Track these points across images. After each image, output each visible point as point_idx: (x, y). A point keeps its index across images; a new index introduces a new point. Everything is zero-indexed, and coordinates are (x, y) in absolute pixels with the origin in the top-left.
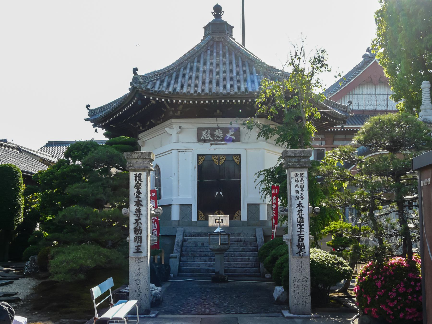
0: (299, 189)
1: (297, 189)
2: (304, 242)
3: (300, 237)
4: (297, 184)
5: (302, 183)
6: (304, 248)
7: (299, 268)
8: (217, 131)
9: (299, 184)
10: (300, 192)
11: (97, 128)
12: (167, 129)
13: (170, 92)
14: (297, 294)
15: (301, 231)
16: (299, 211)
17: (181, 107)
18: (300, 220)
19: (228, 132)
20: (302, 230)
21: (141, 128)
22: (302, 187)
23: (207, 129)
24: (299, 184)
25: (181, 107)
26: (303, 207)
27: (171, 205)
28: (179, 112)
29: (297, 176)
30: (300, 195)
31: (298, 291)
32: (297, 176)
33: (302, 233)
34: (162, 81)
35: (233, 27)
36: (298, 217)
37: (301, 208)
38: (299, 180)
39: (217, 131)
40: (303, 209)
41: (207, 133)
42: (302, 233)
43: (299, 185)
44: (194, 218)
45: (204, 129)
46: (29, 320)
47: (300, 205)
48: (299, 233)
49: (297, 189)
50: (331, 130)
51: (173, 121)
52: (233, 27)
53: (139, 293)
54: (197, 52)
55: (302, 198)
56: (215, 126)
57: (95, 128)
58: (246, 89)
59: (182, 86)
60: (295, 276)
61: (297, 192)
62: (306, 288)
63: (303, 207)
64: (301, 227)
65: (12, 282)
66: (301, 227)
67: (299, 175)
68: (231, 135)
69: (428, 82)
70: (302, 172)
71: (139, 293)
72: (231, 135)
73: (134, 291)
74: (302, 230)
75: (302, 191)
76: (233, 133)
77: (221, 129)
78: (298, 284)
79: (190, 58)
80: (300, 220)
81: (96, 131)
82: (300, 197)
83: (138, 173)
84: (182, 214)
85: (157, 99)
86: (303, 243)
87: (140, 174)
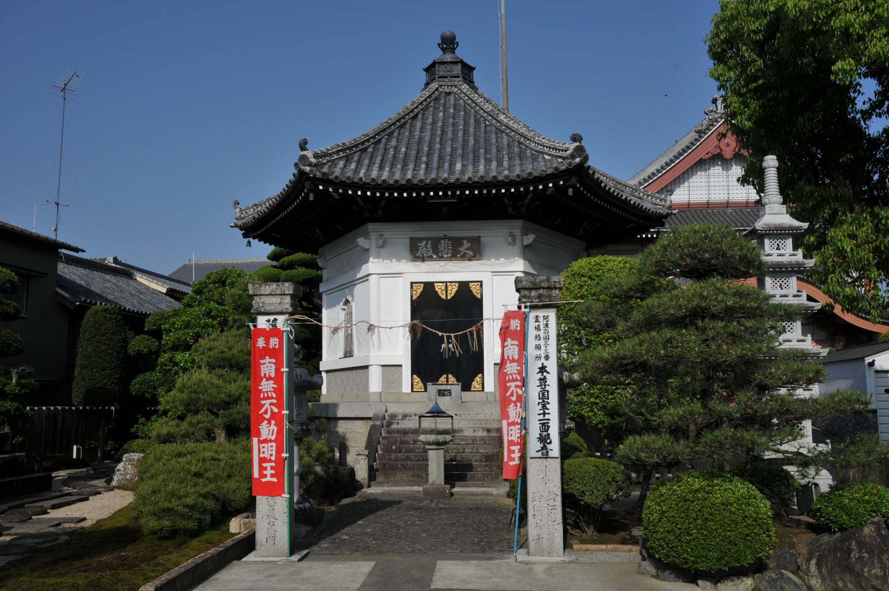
0: (542, 342)
1: (537, 342)
2: (549, 432)
3: (543, 424)
4: (538, 333)
5: (546, 332)
6: (550, 443)
7: (541, 477)
8: (442, 242)
9: (542, 333)
10: (543, 348)
11: (251, 239)
12: (361, 241)
13: (361, 179)
14: (539, 521)
15: (544, 414)
16: (540, 379)
17: (383, 203)
18: (543, 394)
19: (461, 245)
20: (547, 411)
21: (322, 238)
22: (547, 338)
23: (427, 239)
24: (542, 333)
25: (383, 203)
26: (548, 373)
27: (366, 367)
28: (380, 213)
29: (537, 321)
30: (542, 352)
31: (540, 517)
32: (537, 321)
33: (547, 417)
34: (348, 159)
35: (474, 69)
36: (539, 389)
37: (545, 374)
38: (542, 327)
39: (442, 242)
40: (548, 376)
41: (426, 245)
42: (547, 417)
43: (542, 335)
44: (406, 388)
45: (421, 240)
46: (303, 529)
47: (543, 369)
48: (541, 417)
49: (537, 342)
50: (647, 236)
51: (371, 226)
52: (474, 69)
53: (272, 520)
54: (412, 111)
55: (547, 358)
56: (440, 234)
57: (247, 239)
58: (487, 171)
59: (381, 168)
60: (536, 491)
61: (538, 347)
62: (553, 511)
63: (548, 373)
64: (544, 407)
65: (87, 499)
66: (544, 407)
67: (541, 319)
68: (467, 249)
69: (774, 157)
70: (546, 314)
71: (272, 520)
72: (467, 249)
73: (265, 517)
74: (547, 411)
75: (546, 345)
76: (469, 245)
77: (450, 239)
78: (540, 504)
79: (399, 121)
80: (543, 394)
81: (249, 243)
82: (543, 355)
83: (272, 318)
84: (385, 380)
85: (341, 191)
86: (549, 435)
87: (275, 320)
